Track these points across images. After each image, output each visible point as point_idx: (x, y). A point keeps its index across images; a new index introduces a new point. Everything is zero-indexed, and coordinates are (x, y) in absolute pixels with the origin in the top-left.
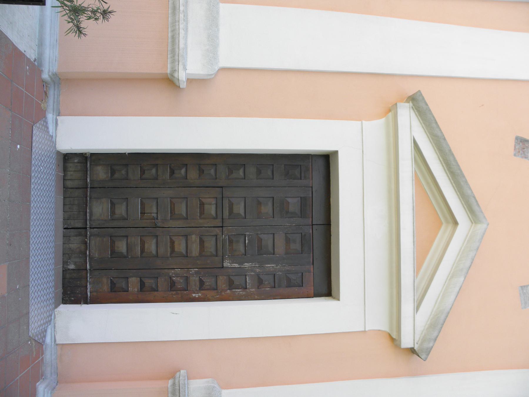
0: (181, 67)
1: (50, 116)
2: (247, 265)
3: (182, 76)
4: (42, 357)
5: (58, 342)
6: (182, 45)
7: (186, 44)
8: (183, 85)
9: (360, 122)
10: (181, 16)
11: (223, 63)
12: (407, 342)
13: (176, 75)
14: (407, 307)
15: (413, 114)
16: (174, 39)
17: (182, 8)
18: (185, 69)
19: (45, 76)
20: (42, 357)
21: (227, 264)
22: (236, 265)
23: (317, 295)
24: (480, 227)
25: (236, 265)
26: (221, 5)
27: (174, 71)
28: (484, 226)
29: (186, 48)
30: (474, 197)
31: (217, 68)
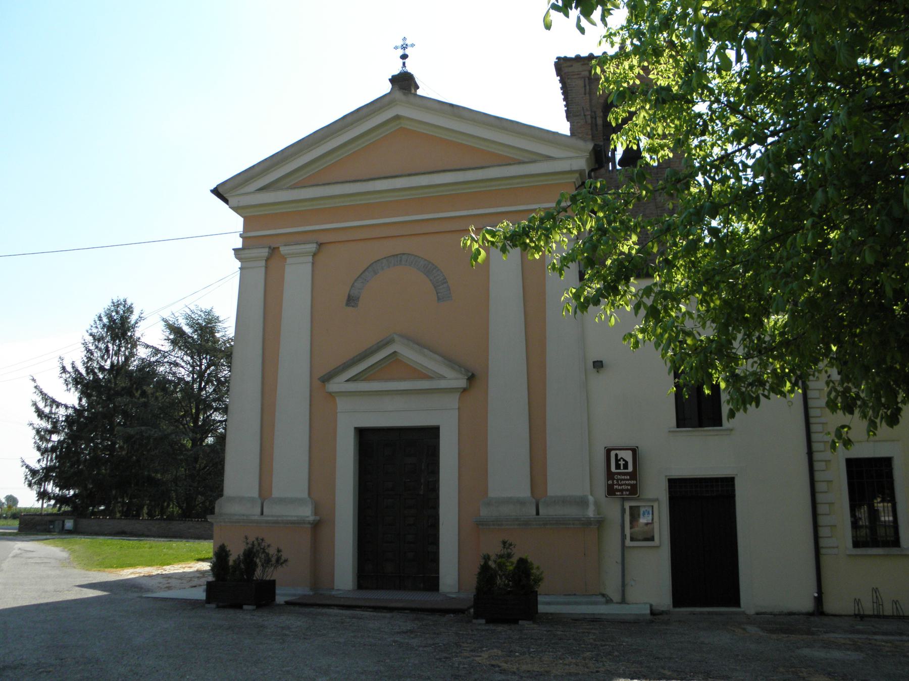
0: (307, 519)
1: (334, 593)
2: (422, 481)
3: (311, 518)
4: (868, 418)
5: (457, 591)
6: (296, 519)
7: (295, 516)
8: (318, 518)
9: (338, 414)
10: (280, 519)
11: (305, 495)
12: (462, 383)
13: (312, 522)
14: (443, 384)
15: (331, 382)
16: (293, 523)
17: (275, 519)
18: (308, 517)
19: (311, 593)
20: (868, 418)
21: (421, 493)
22: (422, 486)
23: (733, 485)
24: (397, 338)
25: (422, 486)
26: (273, 496)
27: (309, 523)
28: (395, 336)
29: (297, 516)
30: (378, 343)
31: (308, 499)
